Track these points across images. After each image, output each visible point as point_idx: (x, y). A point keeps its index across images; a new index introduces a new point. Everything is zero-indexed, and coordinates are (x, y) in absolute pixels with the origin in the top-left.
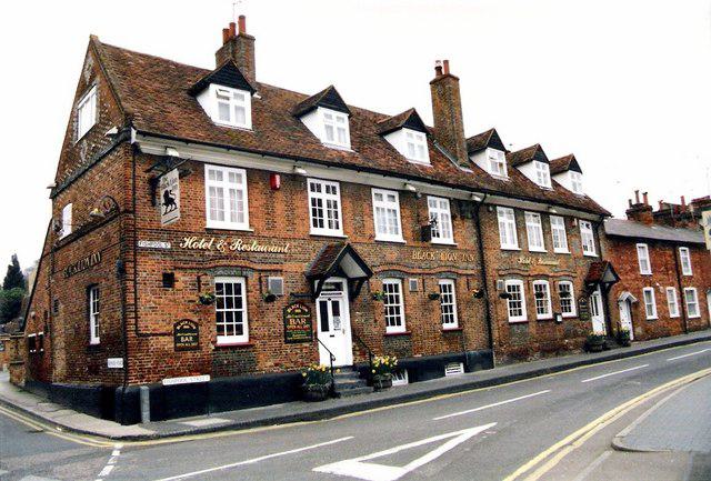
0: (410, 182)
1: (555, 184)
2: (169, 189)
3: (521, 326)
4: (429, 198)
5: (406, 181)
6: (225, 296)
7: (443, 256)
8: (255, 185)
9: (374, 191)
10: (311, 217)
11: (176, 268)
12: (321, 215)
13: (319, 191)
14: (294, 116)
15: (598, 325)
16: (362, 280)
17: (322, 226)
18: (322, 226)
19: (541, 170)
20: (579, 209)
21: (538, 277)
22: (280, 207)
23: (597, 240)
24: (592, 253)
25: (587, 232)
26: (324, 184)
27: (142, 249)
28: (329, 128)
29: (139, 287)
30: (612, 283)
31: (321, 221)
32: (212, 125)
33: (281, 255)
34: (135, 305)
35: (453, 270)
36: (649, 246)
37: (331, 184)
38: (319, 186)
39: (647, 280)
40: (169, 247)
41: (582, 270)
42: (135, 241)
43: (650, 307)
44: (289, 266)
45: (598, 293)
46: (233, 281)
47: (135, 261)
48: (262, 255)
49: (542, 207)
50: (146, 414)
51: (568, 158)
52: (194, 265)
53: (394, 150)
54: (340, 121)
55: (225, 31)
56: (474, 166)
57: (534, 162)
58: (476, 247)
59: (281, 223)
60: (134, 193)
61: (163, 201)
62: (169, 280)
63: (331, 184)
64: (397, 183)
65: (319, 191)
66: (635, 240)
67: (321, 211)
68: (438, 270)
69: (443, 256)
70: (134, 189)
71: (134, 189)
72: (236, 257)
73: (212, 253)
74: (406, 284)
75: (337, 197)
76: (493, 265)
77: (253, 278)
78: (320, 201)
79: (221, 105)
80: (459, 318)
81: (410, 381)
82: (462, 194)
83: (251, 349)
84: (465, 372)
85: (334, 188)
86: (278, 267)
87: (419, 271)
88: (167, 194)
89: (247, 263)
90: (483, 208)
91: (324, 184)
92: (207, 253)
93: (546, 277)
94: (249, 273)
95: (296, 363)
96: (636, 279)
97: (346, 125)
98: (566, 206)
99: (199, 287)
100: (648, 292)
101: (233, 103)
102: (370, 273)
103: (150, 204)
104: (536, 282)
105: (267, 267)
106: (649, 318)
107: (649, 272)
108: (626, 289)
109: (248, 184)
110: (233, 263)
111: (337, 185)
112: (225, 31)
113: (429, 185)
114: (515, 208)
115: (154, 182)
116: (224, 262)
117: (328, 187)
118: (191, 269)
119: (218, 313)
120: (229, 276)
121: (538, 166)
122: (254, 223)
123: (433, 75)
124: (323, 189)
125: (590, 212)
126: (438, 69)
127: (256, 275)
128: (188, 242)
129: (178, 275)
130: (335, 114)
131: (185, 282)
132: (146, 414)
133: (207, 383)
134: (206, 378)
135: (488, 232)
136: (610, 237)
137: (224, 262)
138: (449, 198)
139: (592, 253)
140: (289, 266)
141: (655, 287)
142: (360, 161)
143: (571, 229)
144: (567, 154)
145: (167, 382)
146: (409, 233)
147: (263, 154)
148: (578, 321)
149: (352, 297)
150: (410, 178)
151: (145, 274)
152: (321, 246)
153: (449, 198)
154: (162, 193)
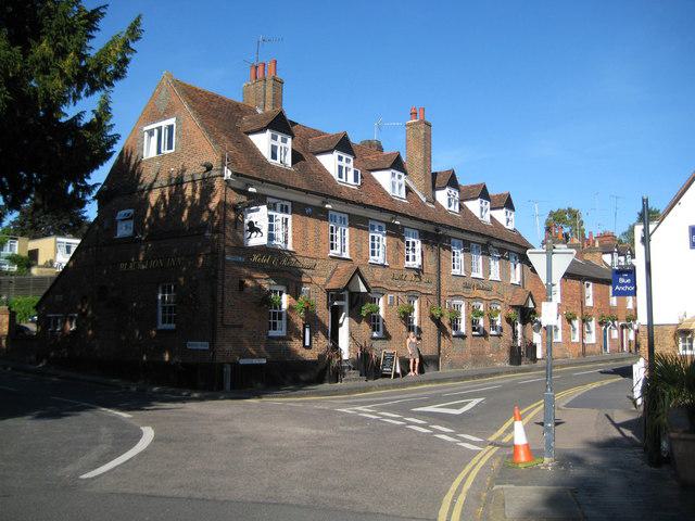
29: (225, 289)
49: (483, 241)
50: (228, 385)
51: (478, 186)
63: (286, 203)
64: (386, 217)
76: (445, 287)
111: (346, 216)
132: (228, 385)
145: (242, 362)
147: (307, 192)
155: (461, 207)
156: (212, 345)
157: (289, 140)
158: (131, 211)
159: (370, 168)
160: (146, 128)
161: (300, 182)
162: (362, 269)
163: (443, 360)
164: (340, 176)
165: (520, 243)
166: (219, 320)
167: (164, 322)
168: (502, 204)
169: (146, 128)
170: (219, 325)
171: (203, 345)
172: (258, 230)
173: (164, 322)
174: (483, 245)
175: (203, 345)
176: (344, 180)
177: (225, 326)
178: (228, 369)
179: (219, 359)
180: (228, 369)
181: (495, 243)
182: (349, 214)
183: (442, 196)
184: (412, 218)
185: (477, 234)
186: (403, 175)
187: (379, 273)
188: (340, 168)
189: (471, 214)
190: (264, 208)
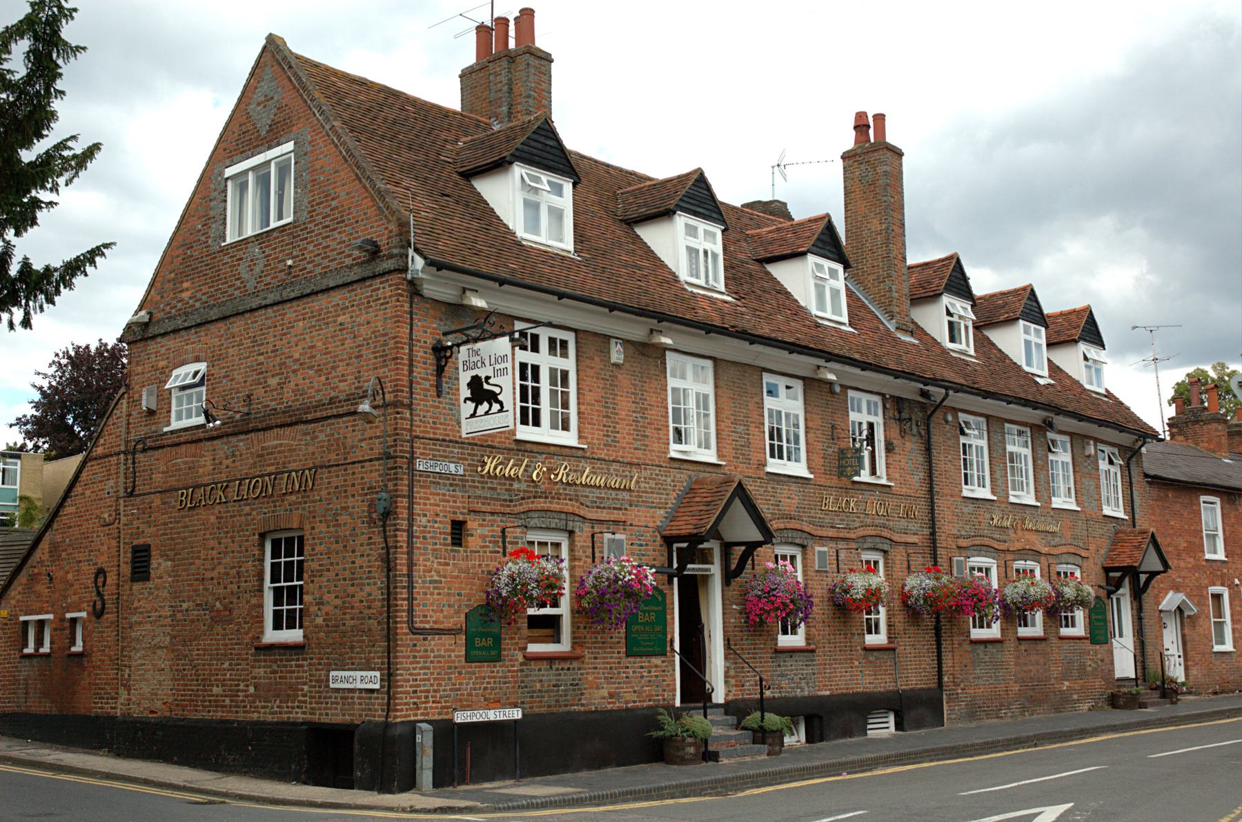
0: (828, 365)
1: (1054, 369)
2: (482, 373)
3: (989, 646)
4: (851, 393)
5: (821, 362)
6: (283, 560)
7: (873, 504)
8: (588, 362)
9: (767, 378)
10: (768, 442)
11: (470, 511)
12: (536, 400)
13: (535, 349)
14: (461, 174)
15: (1124, 665)
16: (752, 547)
17: (537, 423)
18: (537, 423)
19: (1032, 338)
20: (1101, 423)
21: (1024, 553)
22: (625, 406)
23: (1129, 485)
24: (1115, 510)
25: (1109, 472)
26: (544, 334)
27: (425, 474)
28: (532, 207)
29: (418, 543)
30: (1153, 574)
31: (537, 413)
32: (519, 244)
33: (626, 495)
34: (410, 576)
35: (885, 533)
36: (1221, 500)
37: (559, 335)
38: (535, 338)
39: (1216, 571)
40: (461, 472)
41: (1098, 553)
42: (411, 461)
43: (1219, 626)
44: (638, 516)
45: (1125, 591)
46: (550, 538)
47: (411, 497)
48: (597, 492)
49: (1036, 416)
50: (426, 776)
51: (1024, 289)
52: (498, 508)
53: (787, 294)
54: (710, 237)
55: (482, 30)
56: (916, 330)
57: (518, 170)
58: (922, 492)
59: (625, 432)
60: (411, 372)
61: (465, 392)
62: (458, 531)
63: (559, 335)
64: (804, 363)
65: (535, 349)
66: (1193, 488)
67: (536, 392)
68: (861, 532)
69: (873, 504)
70: (411, 365)
71: (411, 365)
72: (558, 496)
73: (523, 486)
74: (809, 556)
75: (568, 364)
76: (948, 527)
77: (582, 538)
78: (536, 369)
79: (527, 203)
80: (890, 626)
81: (810, 739)
82: (907, 389)
83: (575, 664)
84: (897, 729)
85: (564, 344)
86: (616, 515)
87: (831, 533)
88: (475, 383)
89: (569, 507)
90: (938, 415)
91: (544, 334)
92: (516, 485)
93: (1036, 554)
94: (576, 525)
95: (640, 693)
96: (1197, 568)
97: (566, 201)
98: (1081, 418)
99: (504, 548)
100: (1217, 597)
101: (548, 199)
102: (768, 537)
103: (433, 392)
104: (1020, 564)
105: (603, 515)
106: (1217, 648)
107: (1221, 555)
108: (1177, 589)
109: (577, 361)
110: (555, 506)
111: (570, 337)
112: (482, 30)
113: (858, 371)
114: (1071, 434)
115: (442, 354)
116: (541, 504)
117: (552, 341)
118: (492, 513)
119: (867, 619)
120: (548, 529)
121: (691, 231)
122: (725, 452)
123: (848, 141)
124: (544, 345)
125: (1121, 429)
126: (861, 126)
127: (587, 528)
128: (490, 465)
129: (473, 524)
130: (702, 226)
131: (483, 537)
132: (426, 776)
133: (516, 721)
134: (516, 714)
135: (941, 460)
136: (1155, 481)
137: (541, 504)
138: (883, 395)
139: (1115, 510)
140: (638, 516)
141: (1231, 587)
142: (747, 322)
143: (1084, 468)
144: (1078, 305)
145: (460, 717)
146: (818, 461)
147: (612, 307)
148: (1087, 645)
149: (729, 576)
150: (830, 357)
151: (424, 520)
152: (682, 478)
153: (883, 395)
154: (465, 378)
155: (984, 345)
156: (389, 678)
157: (568, 187)
158: (202, 367)
159: (763, 254)
160: (229, 172)
161: (593, 285)
162: (751, 487)
163: (954, 698)
164: (952, 340)
165: (1122, 421)
166: (403, 616)
167: (277, 626)
168: (1077, 333)
169: (229, 172)
170: (403, 628)
171: (369, 679)
172: (492, 397)
173: (277, 626)
174: (1032, 427)
175: (369, 679)
176: (702, 282)
177: (414, 631)
178: (425, 739)
179: (402, 715)
180: (425, 739)
181: (1061, 421)
182: (576, 331)
183: (933, 320)
184: (864, 366)
185: (1026, 403)
186: (839, 268)
187: (790, 500)
188: (1028, 343)
189: (1004, 357)
190: (502, 345)
